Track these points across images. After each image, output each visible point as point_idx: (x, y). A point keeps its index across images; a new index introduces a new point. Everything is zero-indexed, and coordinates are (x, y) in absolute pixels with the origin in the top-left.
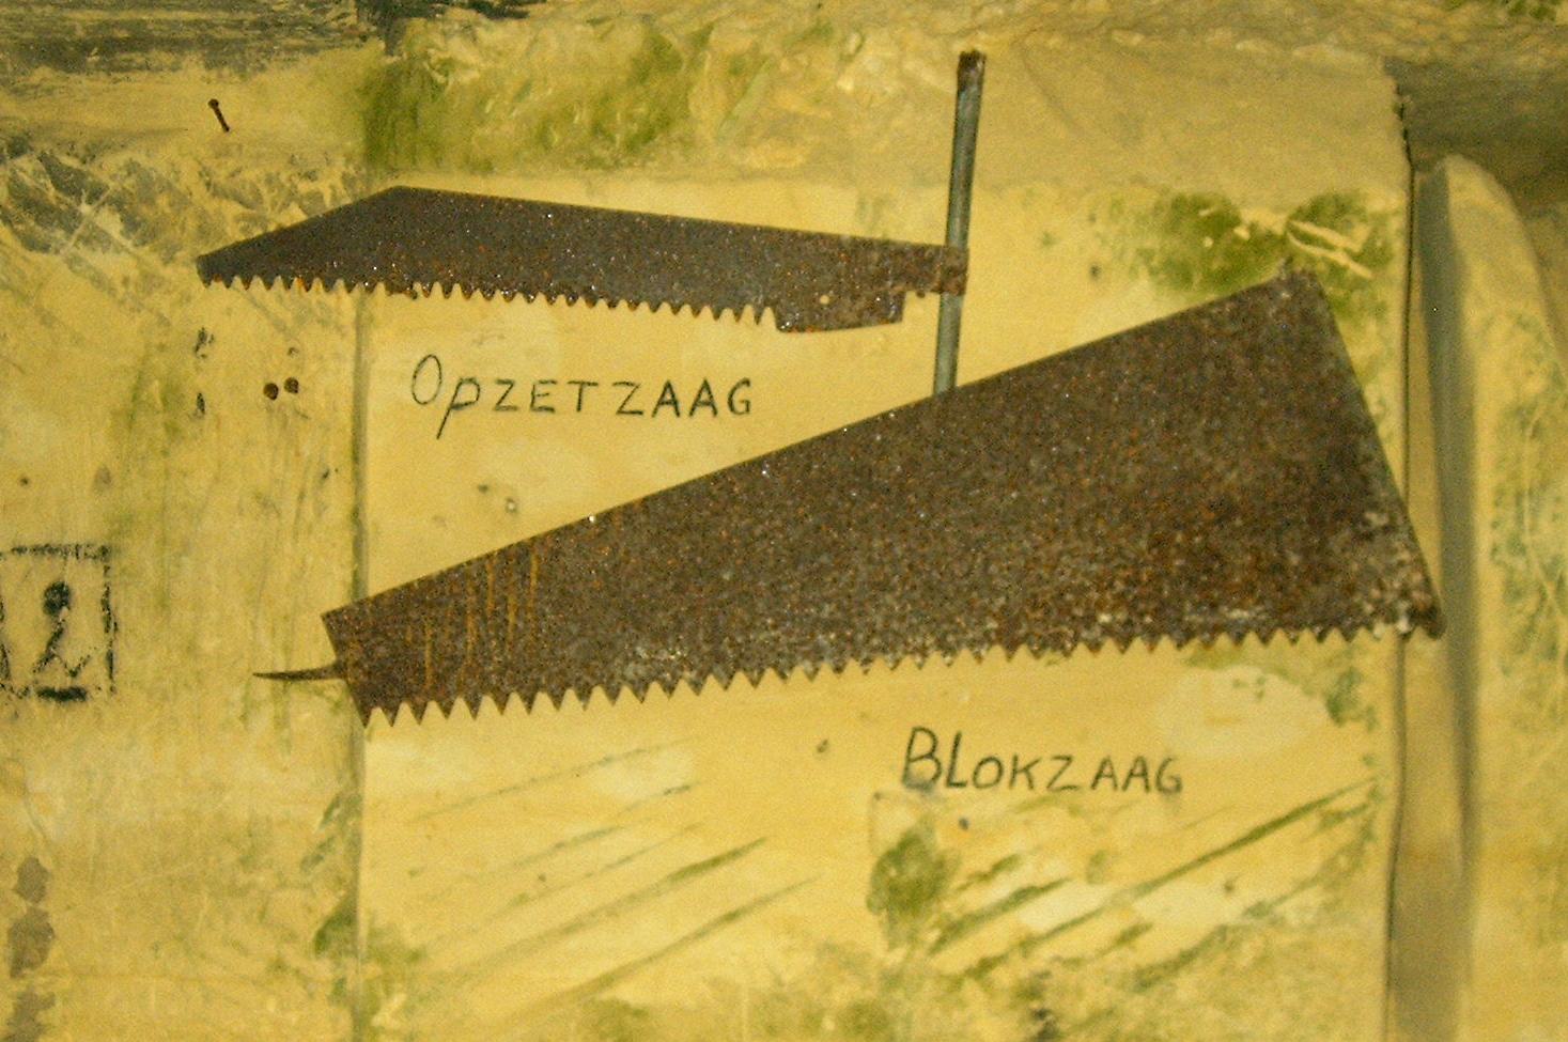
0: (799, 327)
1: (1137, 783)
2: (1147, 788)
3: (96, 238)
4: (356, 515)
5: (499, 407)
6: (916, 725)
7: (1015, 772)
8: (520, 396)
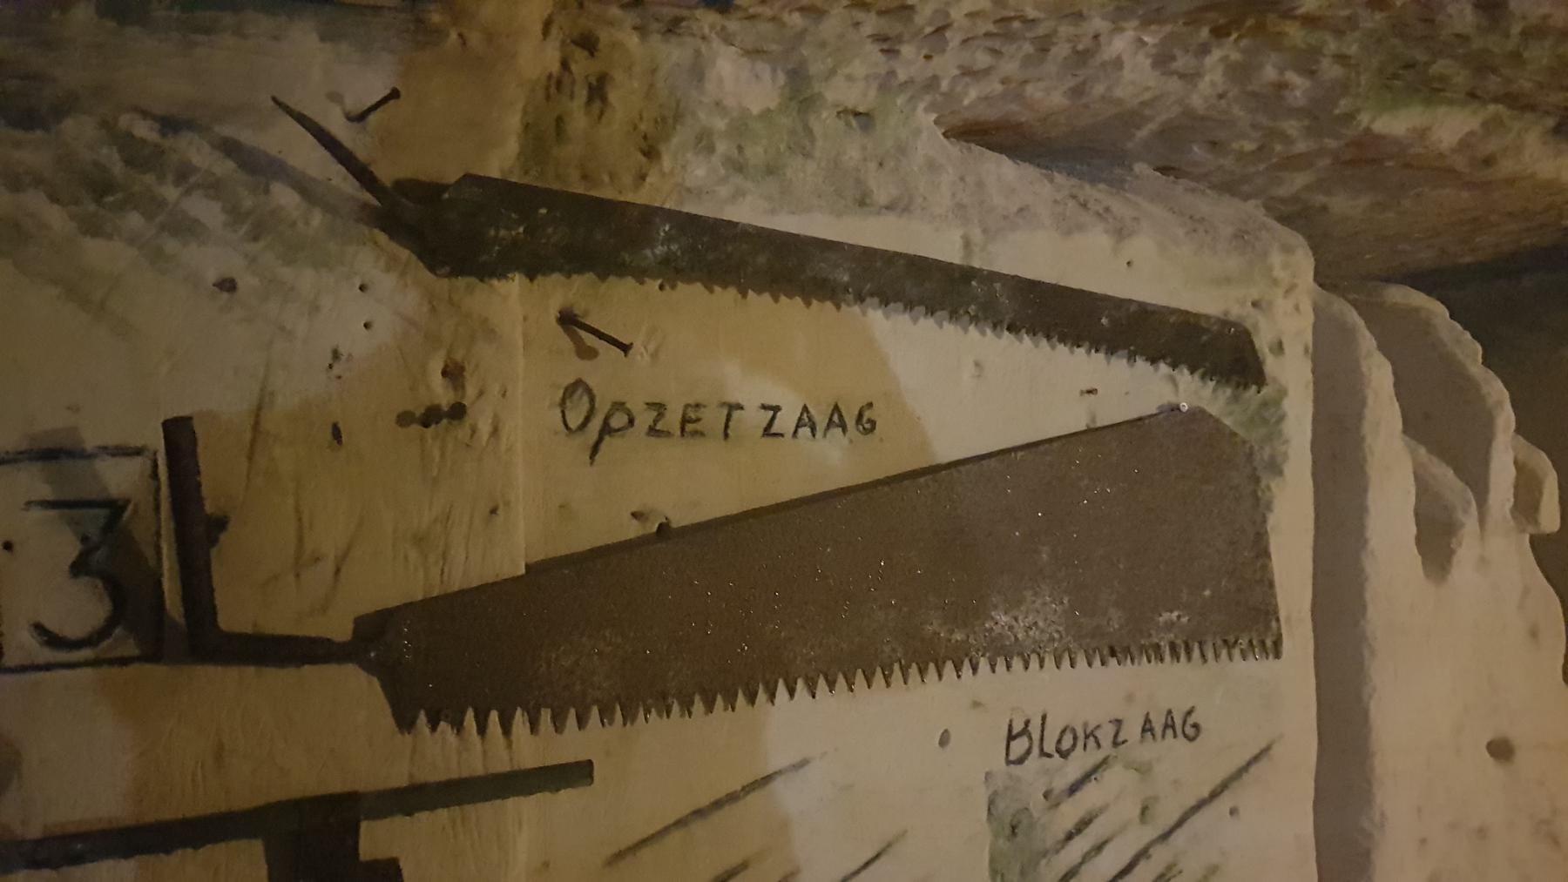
0: (1485, 366)
1: (1169, 732)
2: (1175, 736)
3: (187, 229)
4: (298, 511)
5: (653, 431)
6: (1188, 742)
7: (1087, 737)
8: (785, 422)
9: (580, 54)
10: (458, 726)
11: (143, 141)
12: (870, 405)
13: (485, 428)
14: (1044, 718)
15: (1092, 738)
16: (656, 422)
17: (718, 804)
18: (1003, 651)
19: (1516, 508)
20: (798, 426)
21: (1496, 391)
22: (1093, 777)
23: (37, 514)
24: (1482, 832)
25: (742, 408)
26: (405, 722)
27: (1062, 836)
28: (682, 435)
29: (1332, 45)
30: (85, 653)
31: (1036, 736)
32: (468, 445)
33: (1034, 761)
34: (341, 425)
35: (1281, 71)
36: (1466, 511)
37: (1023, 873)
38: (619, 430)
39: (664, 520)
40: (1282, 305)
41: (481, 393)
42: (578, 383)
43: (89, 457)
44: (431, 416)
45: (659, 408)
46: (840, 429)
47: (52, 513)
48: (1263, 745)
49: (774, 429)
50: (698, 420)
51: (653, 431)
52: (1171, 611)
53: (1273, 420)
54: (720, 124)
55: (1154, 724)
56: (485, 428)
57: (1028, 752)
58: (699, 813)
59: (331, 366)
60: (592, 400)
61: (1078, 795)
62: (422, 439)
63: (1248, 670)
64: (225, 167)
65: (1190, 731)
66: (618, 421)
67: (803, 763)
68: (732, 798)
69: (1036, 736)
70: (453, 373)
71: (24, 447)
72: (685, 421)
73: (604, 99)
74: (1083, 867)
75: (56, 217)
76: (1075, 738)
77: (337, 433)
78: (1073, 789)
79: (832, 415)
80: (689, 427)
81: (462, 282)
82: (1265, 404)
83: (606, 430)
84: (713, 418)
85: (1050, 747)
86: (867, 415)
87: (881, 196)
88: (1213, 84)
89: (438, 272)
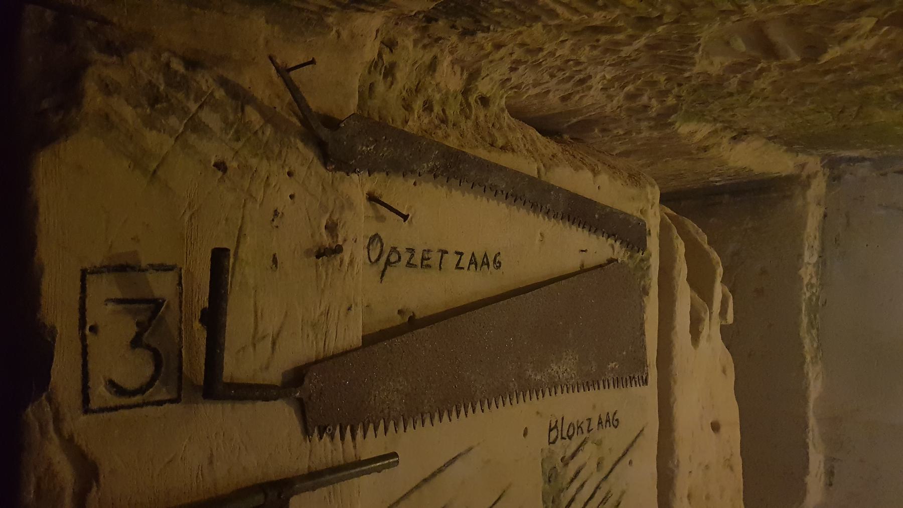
1: (608, 423)
7: (578, 428)
9: (387, 50)
10: (332, 437)
11: (176, 72)
12: (499, 253)
13: (347, 260)
14: (563, 419)
15: (580, 429)
16: (410, 259)
17: (434, 475)
18: (555, 385)
19: (720, 314)
20: (470, 264)
21: (715, 255)
22: (580, 449)
23: (111, 306)
24: (707, 467)
25: (447, 253)
26: (306, 433)
27: (569, 480)
28: (422, 267)
29: (676, 90)
30: (138, 399)
31: (560, 429)
32: (339, 270)
33: (559, 442)
34: (277, 256)
35: (650, 99)
36: (705, 313)
37: (553, 502)
38: (394, 263)
39: (412, 315)
40: (651, 212)
41: (345, 240)
42: (376, 235)
43: (143, 271)
44: (322, 253)
45: (411, 251)
46: (487, 266)
47: (120, 307)
48: (641, 429)
49: (461, 265)
50: (429, 259)
51: (409, 264)
52: (613, 362)
53: (645, 268)
54: (438, 96)
55: (603, 421)
56: (347, 260)
57: (557, 437)
58: (425, 480)
59: (273, 220)
60: (382, 246)
61: (575, 458)
62: (317, 265)
63: (636, 390)
64: (220, 94)
65: (615, 423)
66: (393, 258)
67: (470, 449)
68: (440, 470)
69: (560, 429)
70: (332, 228)
71: (106, 263)
72: (423, 259)
73: (393, 76)
74: (576, 496)
75: (128, 112)
76: (574, 429)
77: (275, 260)
78: (573, 456)
79: (484, 259)
80: (425, 262)
81: (339, 174)
82: (642, 260)
83: (388, 263)
84: (435, 257)
85: (565, 435)
86: (498, 258)
87: (500, 142)
88: (618, 101)
89: (328, 168)
